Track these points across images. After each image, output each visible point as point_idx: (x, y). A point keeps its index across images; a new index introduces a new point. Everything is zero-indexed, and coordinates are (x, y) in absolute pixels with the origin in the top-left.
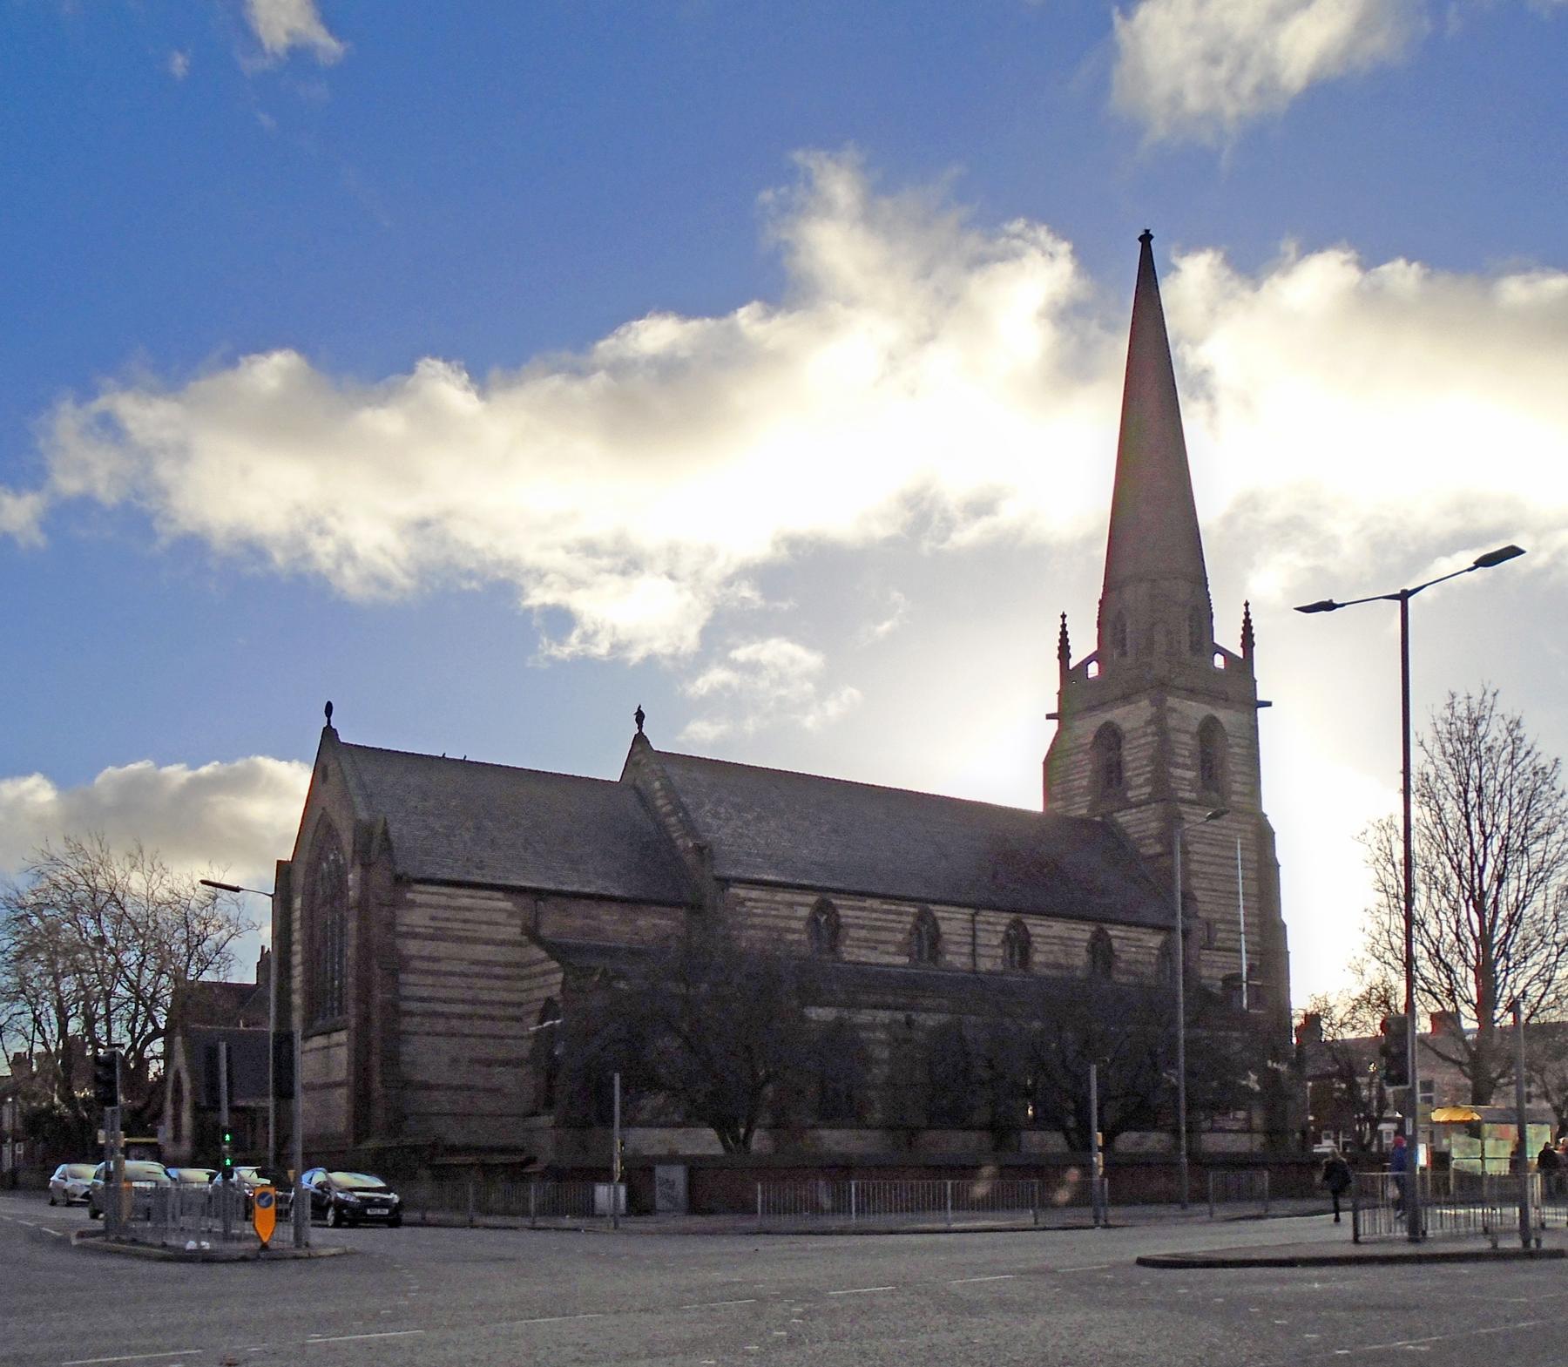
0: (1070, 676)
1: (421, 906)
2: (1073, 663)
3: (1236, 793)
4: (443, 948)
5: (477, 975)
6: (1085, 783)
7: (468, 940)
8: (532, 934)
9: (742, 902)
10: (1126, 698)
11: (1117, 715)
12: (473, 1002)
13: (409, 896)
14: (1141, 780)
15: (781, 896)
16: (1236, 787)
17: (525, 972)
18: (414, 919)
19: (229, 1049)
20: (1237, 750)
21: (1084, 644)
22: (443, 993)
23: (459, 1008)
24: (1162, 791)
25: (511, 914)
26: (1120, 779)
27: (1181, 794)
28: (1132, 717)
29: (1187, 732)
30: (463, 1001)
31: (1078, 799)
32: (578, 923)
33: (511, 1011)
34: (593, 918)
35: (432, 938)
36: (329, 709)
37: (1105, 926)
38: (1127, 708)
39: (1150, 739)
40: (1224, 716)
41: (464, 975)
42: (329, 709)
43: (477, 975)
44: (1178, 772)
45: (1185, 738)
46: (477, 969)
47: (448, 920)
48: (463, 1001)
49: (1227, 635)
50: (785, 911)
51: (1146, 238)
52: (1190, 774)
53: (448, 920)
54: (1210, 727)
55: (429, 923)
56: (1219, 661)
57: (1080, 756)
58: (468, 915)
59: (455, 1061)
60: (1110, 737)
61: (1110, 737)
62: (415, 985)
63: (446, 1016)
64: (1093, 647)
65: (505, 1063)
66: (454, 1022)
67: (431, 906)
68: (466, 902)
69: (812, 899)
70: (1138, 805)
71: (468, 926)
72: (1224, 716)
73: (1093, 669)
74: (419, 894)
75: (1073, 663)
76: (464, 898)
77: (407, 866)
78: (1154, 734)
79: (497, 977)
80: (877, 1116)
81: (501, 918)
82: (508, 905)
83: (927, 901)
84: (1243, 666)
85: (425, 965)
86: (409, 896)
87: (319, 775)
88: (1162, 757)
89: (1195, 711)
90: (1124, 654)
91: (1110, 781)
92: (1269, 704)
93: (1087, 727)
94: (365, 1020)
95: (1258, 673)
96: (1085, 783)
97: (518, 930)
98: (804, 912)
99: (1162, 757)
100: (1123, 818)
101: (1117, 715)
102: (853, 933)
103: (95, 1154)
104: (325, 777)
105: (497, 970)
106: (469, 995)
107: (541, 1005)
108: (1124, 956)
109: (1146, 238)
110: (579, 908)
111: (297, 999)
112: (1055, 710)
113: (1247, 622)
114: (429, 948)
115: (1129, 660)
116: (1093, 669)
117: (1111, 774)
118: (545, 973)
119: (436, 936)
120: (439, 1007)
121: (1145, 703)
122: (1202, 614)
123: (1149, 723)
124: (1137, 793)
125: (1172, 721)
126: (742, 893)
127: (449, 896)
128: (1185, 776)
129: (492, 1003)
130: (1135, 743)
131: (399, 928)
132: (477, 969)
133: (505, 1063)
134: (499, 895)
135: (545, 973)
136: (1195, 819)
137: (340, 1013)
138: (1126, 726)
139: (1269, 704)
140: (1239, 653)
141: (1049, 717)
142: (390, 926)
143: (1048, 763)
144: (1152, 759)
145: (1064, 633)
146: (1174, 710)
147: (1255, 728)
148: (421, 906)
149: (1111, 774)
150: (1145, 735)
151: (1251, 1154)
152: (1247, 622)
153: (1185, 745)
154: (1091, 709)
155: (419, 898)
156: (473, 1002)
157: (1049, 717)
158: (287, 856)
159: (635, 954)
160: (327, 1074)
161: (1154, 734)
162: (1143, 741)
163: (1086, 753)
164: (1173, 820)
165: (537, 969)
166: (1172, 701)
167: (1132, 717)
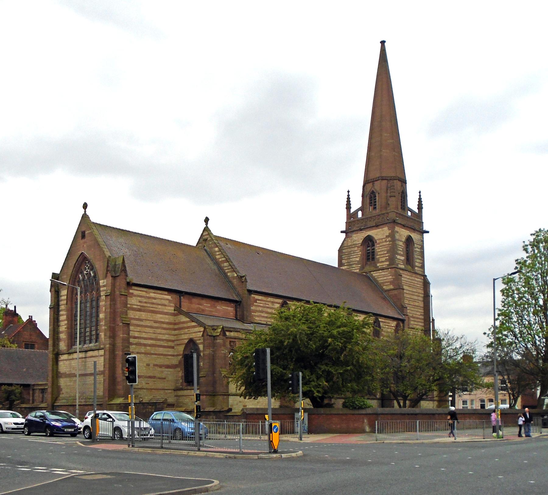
0: (351, 216)
1: (135, 296)
2: (352, 211)
3: (417, 266)
4: (143, 315)
5: (157, 328)
6: (358, 259)
8: (179, 310)
9: (256, 301)
10: (377, 226)
11: (372, 233)
13: (131, 291)
14: (384, 259)
15: (270, 299)
16: (417, 264)
17: (176, 327)
18: (133, 301)
19: (271, 351)
20: (417, 249)
21: (357, 203)
22: (144, 335)
26: (373, 259)
27: (399, 266)
28: (380, 234)
29: (401, 241)
31: (354, 266)
33: (170, 344)
34: (201, 305)
35: (140, 310)
37: (378, 317)
38: (378, 230)
39: (388, 243)
40: (415, 236)
41: (151, 327)
44: (398, 257)
45: (401, 243)
47: (146, 303)
49: (412, 204)
50: (270, 305)
51: (383, 43)
52: (403, 258)
53: (146, 303)
54: (409, 240)
55: (139, 304)
57: (356, 249)
59: (148, 365)
60: (369, 241)
61: (369, 241)
62: (134, 331)
63: (145, 345)
64: (360, 205)
65: (168, 367)
66: (148, 348)
68: (152, 295)
69: (280, 301)
70: (383, 269)
71: (154, 306)
72: (415, 236)
73: (360, 214)
74: (134, 291)
75: (352, 211)
76: (152, 294)
77: (132, 277)
78: (389, 241)
79: (165, 329)
81: (166, 302)
82: (169, 297)
84: (418, 216)
86: (131, 291)
87: (80, 235)
88: (393, 251)
89: (403, 233)
90: (375, 208)
91: (368, 259)
92: (428, 232)
93: (359, 238)
94: (113, 346)
95: (424, 220)
97: (173, 308)
100: (375, 274)
101: (372, 233)
105: (165, 326)
106: (153, 336)
107: (186, 341)
108: (384, 329)
109: (383, 43)
110: (195, 300)
111: (63, 336)
112: (344, 229)
113: (348, 198)
114: (137, 315)
115: (377, 211)
116: (360, 214)
117: (369, 256)
118: (188, 327)
120: (142, 341)
121: (386, 228)
122: (404, 196)
123: (387, 237)
124: (381, 264)
125: (397, 236)
126: (257, 297)
127: (146, 292)
129: (163, 340)
130: (381, 244)
131: (129, 306)
133: (168, 367)
134: (166, 293)
135: (188, 327)
136: (406, 277)
137: (96, 342)
138: (376, 238)
139: (428, 232)
140: (417, 211)
141: (342, 232)
142: (125, 304)
143: (340, 251)
144: (388, 252)
146: (398, 232)
147: (423, 241)
148: (135, 296)
149: (369, 256)
150: (386, 241)
152: (348, 198)
153: (401, 245)
154: (361, 230)
155: (136, 293)
157: (342, 232)
158: (58, 271)
159: (506, 315)
160: (85, 369)
161: (389, 241)
162: (385, 244)
163: (358, 247)
164: (398, 277)
165: (185, 325)
166: (397, 229)
167: (380, 234)
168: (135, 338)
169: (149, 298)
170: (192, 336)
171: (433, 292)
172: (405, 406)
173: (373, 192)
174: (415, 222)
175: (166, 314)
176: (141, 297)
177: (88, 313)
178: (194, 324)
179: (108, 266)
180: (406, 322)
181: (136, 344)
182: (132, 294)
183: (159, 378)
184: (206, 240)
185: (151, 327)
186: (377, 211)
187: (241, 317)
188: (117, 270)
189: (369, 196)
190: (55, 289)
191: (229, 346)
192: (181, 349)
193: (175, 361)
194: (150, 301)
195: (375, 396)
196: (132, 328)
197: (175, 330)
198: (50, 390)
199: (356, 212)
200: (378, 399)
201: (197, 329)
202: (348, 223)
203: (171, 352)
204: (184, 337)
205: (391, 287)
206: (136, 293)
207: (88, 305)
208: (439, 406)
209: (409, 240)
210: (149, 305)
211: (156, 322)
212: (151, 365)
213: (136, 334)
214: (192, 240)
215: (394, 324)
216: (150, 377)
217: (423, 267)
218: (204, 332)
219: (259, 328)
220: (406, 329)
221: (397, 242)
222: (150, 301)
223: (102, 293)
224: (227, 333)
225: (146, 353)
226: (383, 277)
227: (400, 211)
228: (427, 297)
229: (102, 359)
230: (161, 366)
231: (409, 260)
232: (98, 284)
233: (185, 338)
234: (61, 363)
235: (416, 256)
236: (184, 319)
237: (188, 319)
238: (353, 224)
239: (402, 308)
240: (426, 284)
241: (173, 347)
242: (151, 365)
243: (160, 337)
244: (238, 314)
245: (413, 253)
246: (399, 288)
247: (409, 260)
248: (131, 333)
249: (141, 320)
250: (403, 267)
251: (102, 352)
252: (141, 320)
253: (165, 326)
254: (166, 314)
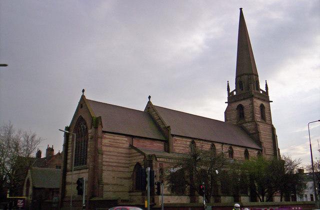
0: (230, 95)
1: (107, 138)
4: (112, 149)
5: (119, 156)
7: (117, 147)
12: (118, 163)
14: (249, 117)
15: (184, 139)
18: (105, 141)
21: (233, 88)
23: (115, 164)
24: (253, 120)
25: (127, 141)
26: (243, 116)
28: (245, 103)
30: (116, 162)
32: (142, 144)
36: (83, 91)
41: (116, 156)
42: (83, 91)
43: (119, 156)
45: (258, 108)
46: (119, 155)
48: (116, 162)
49: (262, 87)
50: (185, 143)
51: (241, 9)
54: (262, 107)
56: (261, 92)
58: (118, 141)
59: (114, 177)
60: (241, 108)
65: (125, 178)
66: (114, 168)
67: (110, 139)
68: (118, 138)
69: (190, 140)
70: (249, 122)
72: (264, 104)
73: (235, 93)
74: (107, 136)
76: (116, 137)
80: (187, 194)
82: (126, 139)
83: (214, 142)
85: (109, 153)
93: (235, 105)
96: (235, 117)
98: (188, 143)
99: (253, 112)
100: (245, 125)
102: (105, 153)
103: (208, 201)
104: (82, 107)
107: (135, 164)
109: (241, 9)
110: (142, 141)
114: (108, 149)
115: (244, 91)
116: (235, 93)
118: (136, 156)
119: (110, 146)
120: (110, 164)
126: (177, 138)
128: (258, 116)
132: (119, 155)
133: (125, 178)
134: (125, 137)
135: (136, 156)
140: (265, 91)
145: (228, 85)
151: (186, 204)
152: (228, 85)
154: (236, 101)
155: (107, 136)
156: (118, 163)
164: (256, 125)
165: (135, 155)
166: (255, 100)
167: (245, 103)
168: (106, 162)
169: (114, 139)
170: (139, 161)
171: (277, 133)
172: (263, 201)
173: (241, 82)
174: (265, 96)
175: (124, 148)
176: (110, 139)
177: (83, 148)
178: (139, 154)
179: (92, 122)
180: (263, 151)
181: (107, 166)
182: (105, 137)
183: (120, 185)
184: (149, 108)
185: (116, 156)
186: (244, 91)
187: (167, 150)
188: (97, 123)
189: (239, 83)
190: (67, 136)
191: (159, 167)
192: (132, 168)
193: (129, 175)
194: (116, 141)
195: (247, 194)
196: (104, 156)
197: (129, 157)
198: (60, 192)
199: (233, 92)
200: (232, 196)
201: (141, 157)
202: (229, 98)
203: (127, 170)
204: (134, 161)
205: (254, 132)
206: (107, 136)
207: (83, 143)
208: (191, 202)
209: (262, 107)
210: (114, 143)
211: (118, 153)
212: (116, 178)
213: (108, 160)
214: (142, 108)
215: (256, 152)
216: (115, 185)
217: (271, 120)
218: (144, 158)
219: (177, 156)
220: (264, 155)
221: (256, 107)
222: (116, 141)
223: (89, 137)
224: (158, 159)
225: (113, 171)
226: (249, 126)
227: (256, 91)
228: (274, 137)
229: (87, 174)
230: (121, 178)
231: (263, 117)
232: (87, 131)
233: (135, 162)
234: (67, 177)
235: (267, 114)
236: (134, 151)
237: (136, 151)
238: (231, 99)
239: (259, 143)
240: (273, 129)
241: (128, 167)
242: (116, 178)
243: (120, 161)
244: (166, 148)
245: (265, 112)
246: (258, 132)
247: (263, 117)
248: (104, 159)
249: (111, 152)
250: (260, 120)
251: (87, 170)
252: (111, 152)
253: (123, 155)
254: (124, 148)
